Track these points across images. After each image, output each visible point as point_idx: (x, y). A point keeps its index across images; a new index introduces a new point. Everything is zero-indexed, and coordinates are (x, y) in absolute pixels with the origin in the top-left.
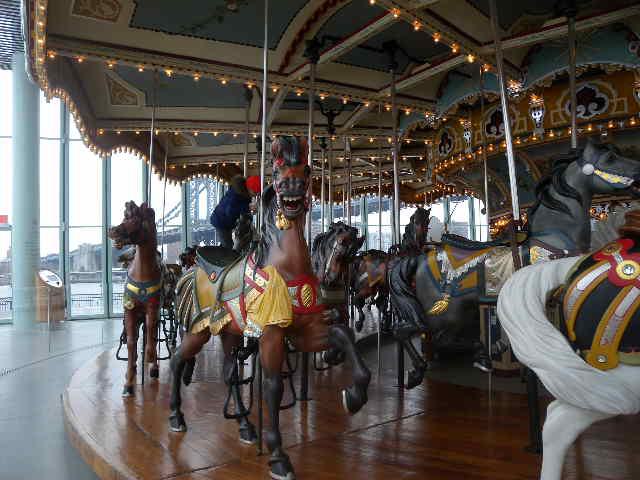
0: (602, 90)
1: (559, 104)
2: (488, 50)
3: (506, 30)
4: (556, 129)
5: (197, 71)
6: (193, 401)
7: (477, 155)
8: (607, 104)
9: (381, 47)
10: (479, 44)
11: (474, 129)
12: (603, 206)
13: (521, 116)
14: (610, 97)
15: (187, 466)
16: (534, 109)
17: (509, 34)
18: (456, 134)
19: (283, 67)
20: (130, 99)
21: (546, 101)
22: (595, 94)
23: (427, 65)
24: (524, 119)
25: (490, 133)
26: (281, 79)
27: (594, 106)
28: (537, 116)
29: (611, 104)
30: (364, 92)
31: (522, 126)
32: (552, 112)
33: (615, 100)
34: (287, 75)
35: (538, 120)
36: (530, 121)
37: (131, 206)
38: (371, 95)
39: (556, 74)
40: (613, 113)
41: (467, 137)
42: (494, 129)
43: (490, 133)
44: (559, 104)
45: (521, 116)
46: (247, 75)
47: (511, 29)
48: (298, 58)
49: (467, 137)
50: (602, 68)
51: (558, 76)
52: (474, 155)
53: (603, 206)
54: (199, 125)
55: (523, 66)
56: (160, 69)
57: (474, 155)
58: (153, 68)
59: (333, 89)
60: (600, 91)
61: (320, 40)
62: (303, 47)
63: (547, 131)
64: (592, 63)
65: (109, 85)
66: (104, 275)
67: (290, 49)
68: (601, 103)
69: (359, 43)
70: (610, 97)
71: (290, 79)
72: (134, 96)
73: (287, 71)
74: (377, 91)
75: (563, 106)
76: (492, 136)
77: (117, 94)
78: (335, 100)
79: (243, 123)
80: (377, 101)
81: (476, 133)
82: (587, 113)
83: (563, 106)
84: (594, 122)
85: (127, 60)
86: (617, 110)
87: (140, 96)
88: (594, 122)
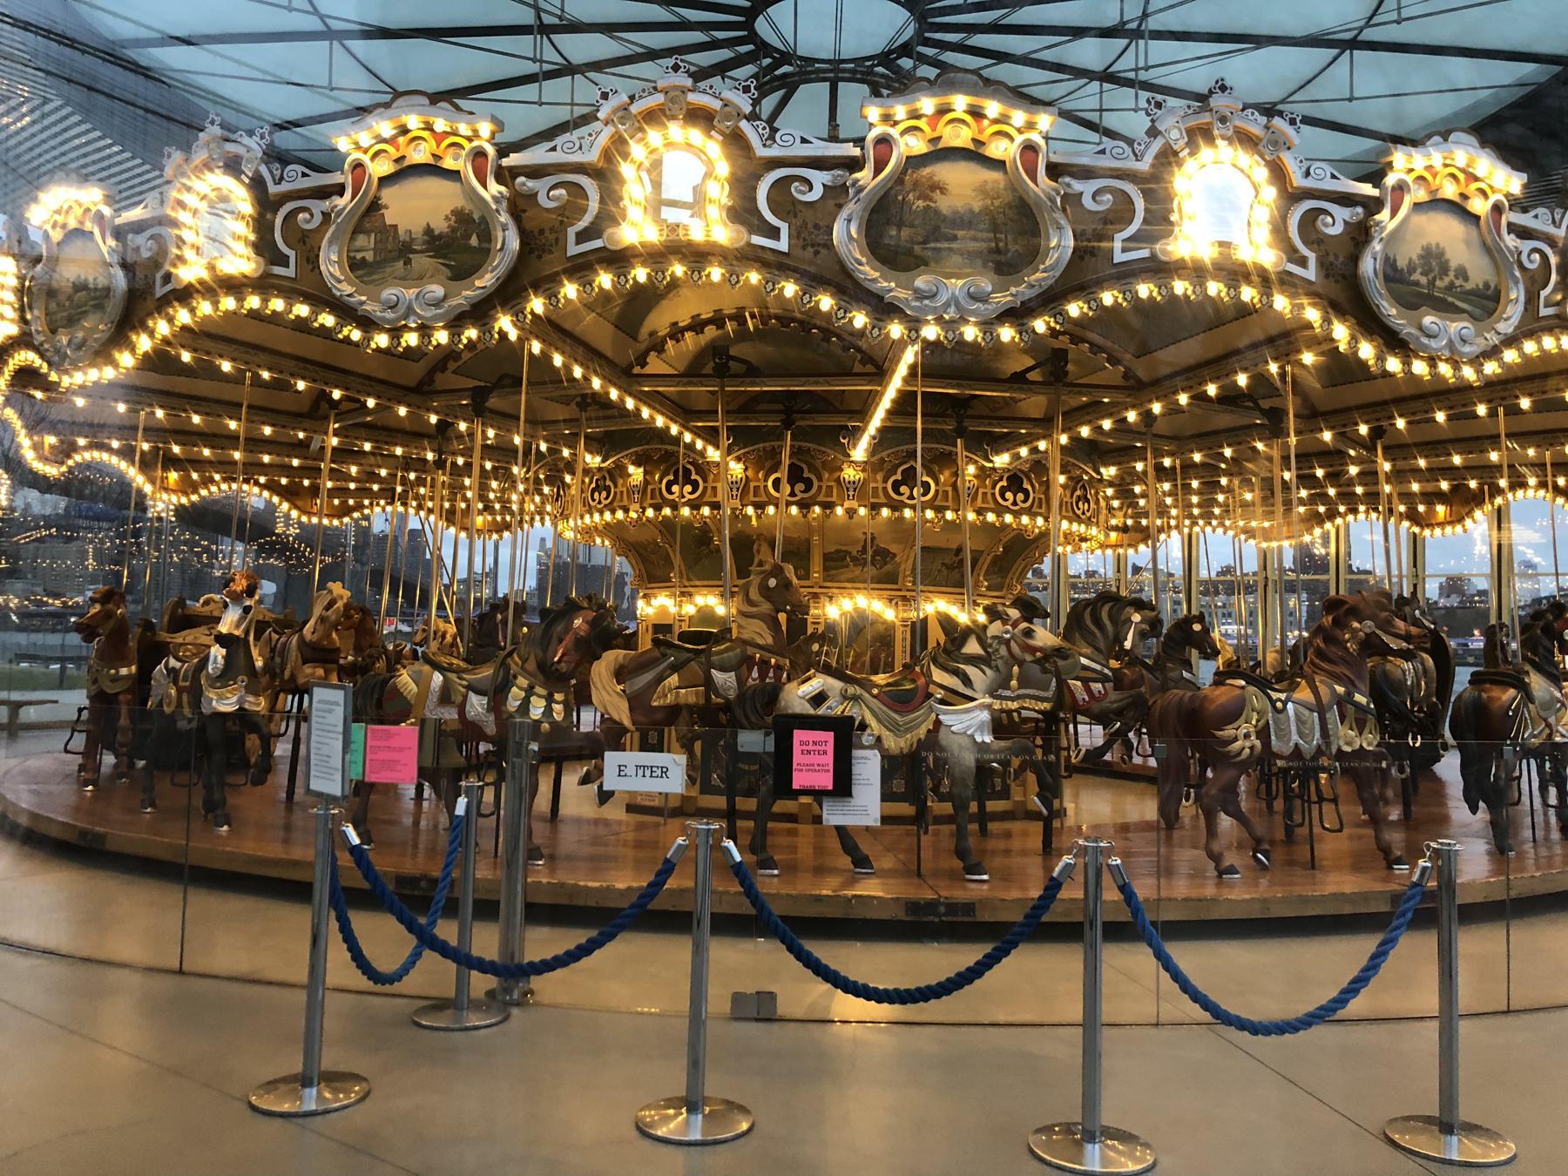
8: (816, 484)
40: (821, 498)
42: (675, 488)
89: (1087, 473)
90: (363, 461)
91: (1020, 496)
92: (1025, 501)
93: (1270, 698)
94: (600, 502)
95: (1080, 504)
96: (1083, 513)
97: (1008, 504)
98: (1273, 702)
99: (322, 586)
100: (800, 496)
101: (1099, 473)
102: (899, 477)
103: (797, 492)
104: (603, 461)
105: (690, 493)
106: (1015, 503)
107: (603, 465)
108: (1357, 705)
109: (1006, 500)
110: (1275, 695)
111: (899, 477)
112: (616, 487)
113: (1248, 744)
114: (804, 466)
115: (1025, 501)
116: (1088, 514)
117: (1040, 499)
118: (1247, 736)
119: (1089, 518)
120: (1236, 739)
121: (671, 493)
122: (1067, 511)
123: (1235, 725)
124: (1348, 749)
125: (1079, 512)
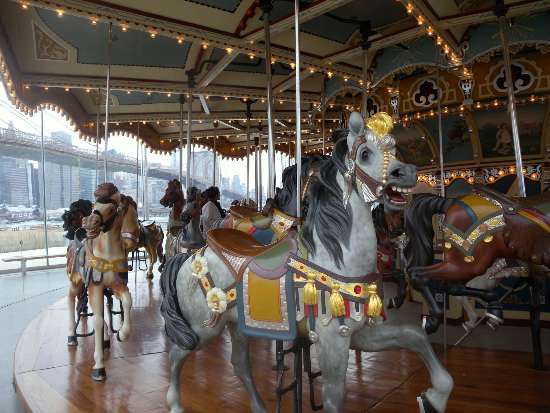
0: (528, 67)
1: (487, 78)
2: (445, 24)
3: (344, 43)
4: (482, 101)
5: (155, 28)
6: (230, 364)
7: (402, 122)
8: (532, 79)
11: (402, 97)
12: (535, 167)
14: (535, 74)
18: (382, 102)
19: (239, 29)
20: (59, 54)
21: (476, 75)
22: (521, 71)
23: (379, 35)
24: (454, 90)
26: (235, 41)
27: (520, 82)
28: (467, 88)
29: (536, 81)
30: (310, 58)
31: (451, 96)
32: (480, 86)
33: (447, 91)
34: (241, 37)
35: (467, 91)
36: (459, 91)
38: (316, 61)
40: (537, 89)
41: (395, 105)
42: (423, 99)
44: (487, 78)
45: (384, 104)
46: (203, 36)
47: (348, 42)
48: (254, 23)
49: (395, 105)
50: (537, 48)
51: (525, 46)
52: (399, 121)
53: (535, 167)
54: (132, 83)
55: (463, 40)
56: (115, 23)
57: (399, 121)
58: (108, 22)
60: (526, 69)
63: (475, 102)
65: (37, 37)
66: (45, 228)
68: (526, 79)
70: (535, 74)
71: (244, 42)
72: (63, 51)
73: (242, 33)
74: (320, 58)
75: (491, 80)
76: (422, 104)
77: (45, 49)
80: (322, 68)
81: (404, 101)
82: (427, 103)
83: (491, 80)
84: (435, 108)
85: (80, 11)
86: (448, 100)
87: (72, 52)
102: (419, 91)
103: (430, 100)
121: (419, 102)
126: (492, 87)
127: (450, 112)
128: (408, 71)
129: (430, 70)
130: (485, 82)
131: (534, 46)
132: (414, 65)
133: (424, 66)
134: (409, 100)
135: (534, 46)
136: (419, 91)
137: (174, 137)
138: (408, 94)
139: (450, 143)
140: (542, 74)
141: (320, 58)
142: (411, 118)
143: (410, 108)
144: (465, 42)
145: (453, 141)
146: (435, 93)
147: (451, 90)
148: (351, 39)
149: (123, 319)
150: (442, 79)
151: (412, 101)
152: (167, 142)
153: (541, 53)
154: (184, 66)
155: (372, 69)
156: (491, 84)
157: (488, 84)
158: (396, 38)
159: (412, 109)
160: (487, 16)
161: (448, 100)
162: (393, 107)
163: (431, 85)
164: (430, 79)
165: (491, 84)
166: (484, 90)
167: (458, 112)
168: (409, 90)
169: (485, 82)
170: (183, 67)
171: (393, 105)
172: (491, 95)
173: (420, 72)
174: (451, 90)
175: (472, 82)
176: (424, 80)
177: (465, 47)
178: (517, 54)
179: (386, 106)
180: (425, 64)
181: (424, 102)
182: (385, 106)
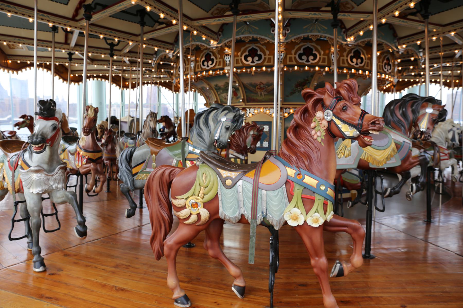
0: (262, 50)
1: (293, 52)
3: (208, 12)
8: (263, 57)
9: (135, 13)
10: (192, 19)
11: (196, 61)
13: (220, 58)
14: (265, 54)
15: (28, 252)
16: (226, 55)
17: (208, 15)
24: (221, 60)
25: (204, 65)
29: (265, 58)
32: (288, 56)
37: (58, 32)
39: (253, 37)
40: (266, 63)
42: (354, 60)
43: (204, 65)
44: (293, 52)
45: (220, 58)
47: (210, 12)
59: (108, 32)
60: (316, 51)
61: (93, 6)
62: (82, 11)
64: (255, 36)
67: (78, 6)
68: (260, 57)
69: (123, 9)
70: (265, 54)
75: (295, 54)
76: (249, 63)
78: (24, 62)
79: (51, 42)
81: (197, 64)
82: (253, 62)
83: (295, 54)
86: (267, 62)
88: (257, 67)
89: (392, 48)
90: (12, 58)
91: (359, 61)
92: (361, 63)
93: (220, 175)
94: (208, 66)
95: (386, 66)
96: (388, 71)
97: (354, 64)
98: (223, 181)
99: (170, 142)
100: (256, 63)
101: (397, 48)
102: (247, 53)
103: (254, 61)
104: (218, 44)
105: (258, 61)
106: (357, 64)
107: (218, 45)
108: (306, 187)
109: (353, 62)
110: (225, 173)
111: (301, 51)
112: (216, 59)
113: (195, 211)
114: (212, 54)
115: (361, 63)
116: (390, 71)
117: (368, 63)
118: (195, 205)
119: (390, 73)
120: (184, 207)
122: (380, 69)
123: (185, 196)
124: (292, 223)
125: (386, 70)
126: (295, 58)
127: (247, 71)
128: (246, 39)
129: (262, 41)
130: (292, 54)
131: (241, 39)
132: (251, 36)
133: (258, 38)
134: (239, 58)
135: (257, 38)
136: (247, 53)
137: (23, 59)
138: (239, 54)
139: (294, 89)
140: (269, 55)
141: (192, 19)
142: (214, 73)
143: (239, 63)
144: (288, 27)
145: (297, 89)
146: (315, 57)
147: (270, 56)
148: (213, 10)
149: (33, 244)
150: (264, 48)
151: (241, 59)
152: (15, 63)
153: (329, 43)
154: (68, 3)
155: (220, 33)
156: (295, 56)
157: (293, 56)
158: (253, 17)
159: (241, 65)
160: (342, 16)
161: (267, 62)
162: (226, 61)
163: (257, 51)
164: (256, 46)
165: (295, 56)
166: (291, 60)
167: (251, 71)
168: (240, 51)
169: (292, 54)
170: (66, 3)
171: (226, 60)
172: (294, 63)
173: (254, 41)
174: (270, 56)
175: (284, 53)
176: (253, 46)
177: (288, 31)
178: (248, 42)
179: (221, 60)
180: (259, 36)
181: (306, 60)
182: (220, 60)
